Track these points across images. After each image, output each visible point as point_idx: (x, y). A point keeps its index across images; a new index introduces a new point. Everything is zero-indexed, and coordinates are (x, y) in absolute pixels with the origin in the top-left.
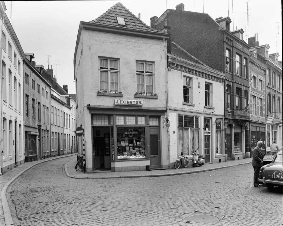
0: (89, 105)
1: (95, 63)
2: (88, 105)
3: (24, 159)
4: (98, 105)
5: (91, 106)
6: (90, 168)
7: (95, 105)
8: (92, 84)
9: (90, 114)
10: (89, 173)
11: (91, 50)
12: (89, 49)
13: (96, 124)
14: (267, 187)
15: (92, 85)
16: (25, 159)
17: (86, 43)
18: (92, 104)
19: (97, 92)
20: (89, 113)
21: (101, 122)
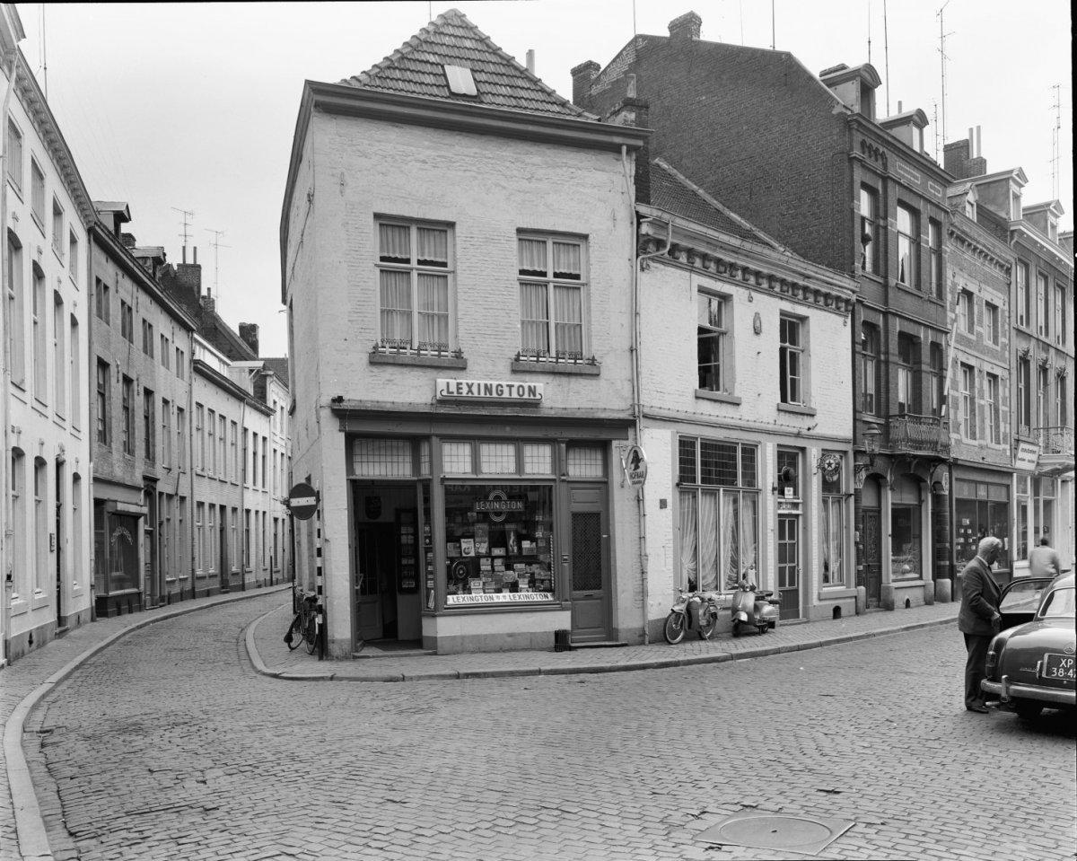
0: (340, 399)
1: (360, 238)
2: (334, 401)
3: (92, 608)
4: (372, 401)
5: (345, 405)
6: (342, 641)
7: (361, 401)
8: (351, 319)
9: (343, 434)
10: (337, 658)
11: (348, 191)
12: (338, 188)
13: (365, 473)
14: (1016, 714)
15: (350, 324)
16: (94, 604)
17: (329, 165)
18: (348, 398)
19: (367, 352)
20: (340, 431)
21: (383, 465)
